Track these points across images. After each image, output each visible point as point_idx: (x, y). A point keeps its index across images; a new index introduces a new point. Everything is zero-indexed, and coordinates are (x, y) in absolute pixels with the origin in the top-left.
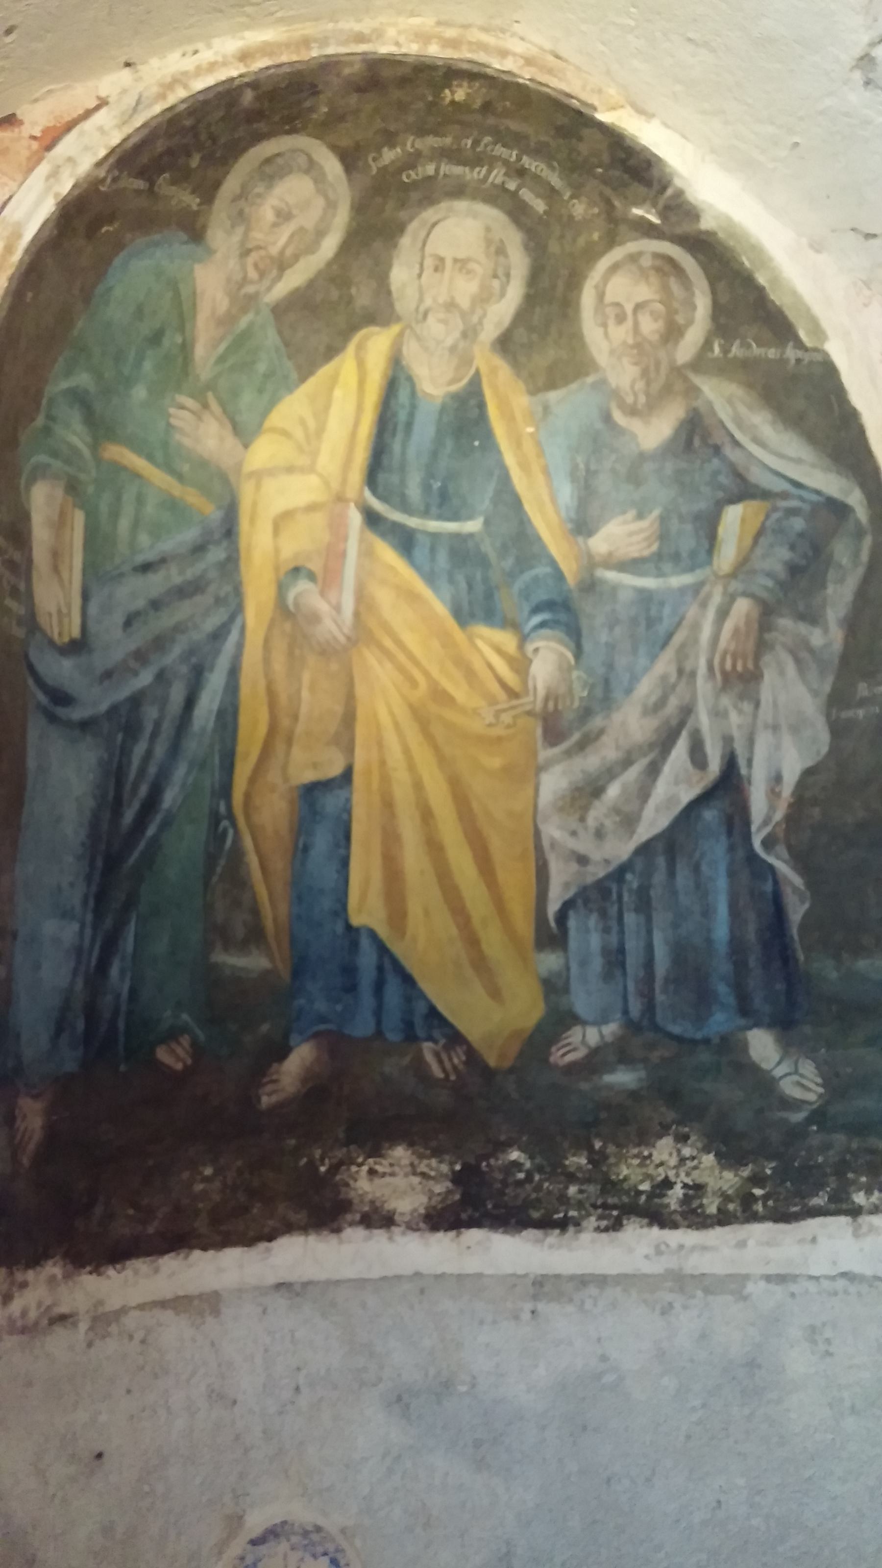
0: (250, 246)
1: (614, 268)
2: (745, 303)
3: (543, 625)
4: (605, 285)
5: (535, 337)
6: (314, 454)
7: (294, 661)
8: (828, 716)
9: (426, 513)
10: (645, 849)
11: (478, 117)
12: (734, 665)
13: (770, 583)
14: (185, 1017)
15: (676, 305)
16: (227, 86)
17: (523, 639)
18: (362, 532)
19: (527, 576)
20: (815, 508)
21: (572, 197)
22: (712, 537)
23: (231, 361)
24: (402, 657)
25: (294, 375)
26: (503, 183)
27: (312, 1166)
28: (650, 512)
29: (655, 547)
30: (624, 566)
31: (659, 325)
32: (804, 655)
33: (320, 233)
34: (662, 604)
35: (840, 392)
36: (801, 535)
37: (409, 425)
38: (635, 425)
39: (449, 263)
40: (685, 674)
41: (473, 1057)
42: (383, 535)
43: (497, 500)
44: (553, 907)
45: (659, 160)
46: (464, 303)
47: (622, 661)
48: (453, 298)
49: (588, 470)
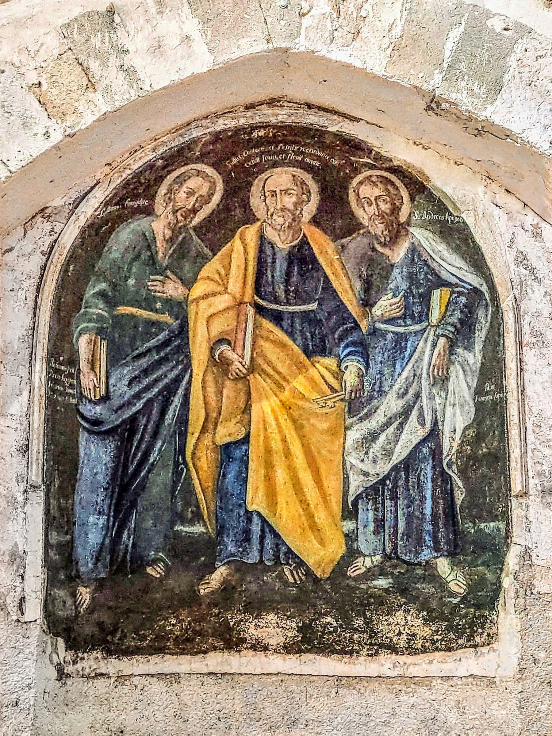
0: (176, 208)
3: (349, 354)
9: (288, 303)
10: (395, 468)
14: (161, 554)
27: (227, 622)
31: (388, 206)
41: (309, 573)
44: (351, 499)
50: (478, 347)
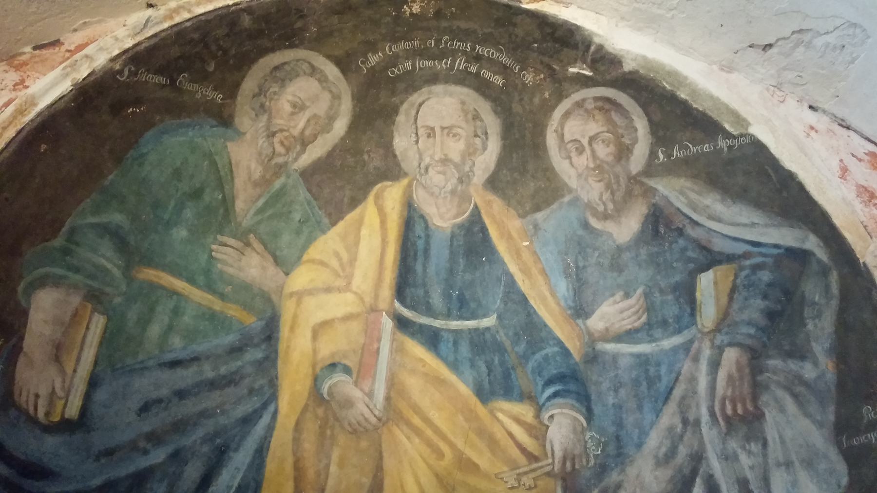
1: (567, 115)
2: (674, 115)
3: (555, 395)
4: (562, 129)
5: (516, 175)
6: (349, 278)
7: (324, 438)
8: (839, 444)
9: (448, 316)
11: (434, 23)
12: (734, 409)
13: (752, 331)
15: (620, 131)
16: (225, 11)
17: (539, 410)
18: (394, 334)
19: (538, 356)
20: (778, 259)
21: (521, 70)
22: (692, 302)
23: (269, 212)
24: (429, 432)
25: (326, 221)
26: (466, 68)
28: (635, 290)
29: (644, 318)
30: (619, 338)
31: (612, 148)
32: (800, 389)
33: (331, 119)
34: (658, 364)
35: (774, 162)
36: (770, 285)
37: (426, 251)
38: (609, 227)
39: (438, 130)
40: (690, 424)
42: (413, 335)
43: (505, 301)
45: (578, 28)
46: (456, 157)
47: (630, 420)
48: (446, 155)
49: (577, 267)
50: (820, 348)
